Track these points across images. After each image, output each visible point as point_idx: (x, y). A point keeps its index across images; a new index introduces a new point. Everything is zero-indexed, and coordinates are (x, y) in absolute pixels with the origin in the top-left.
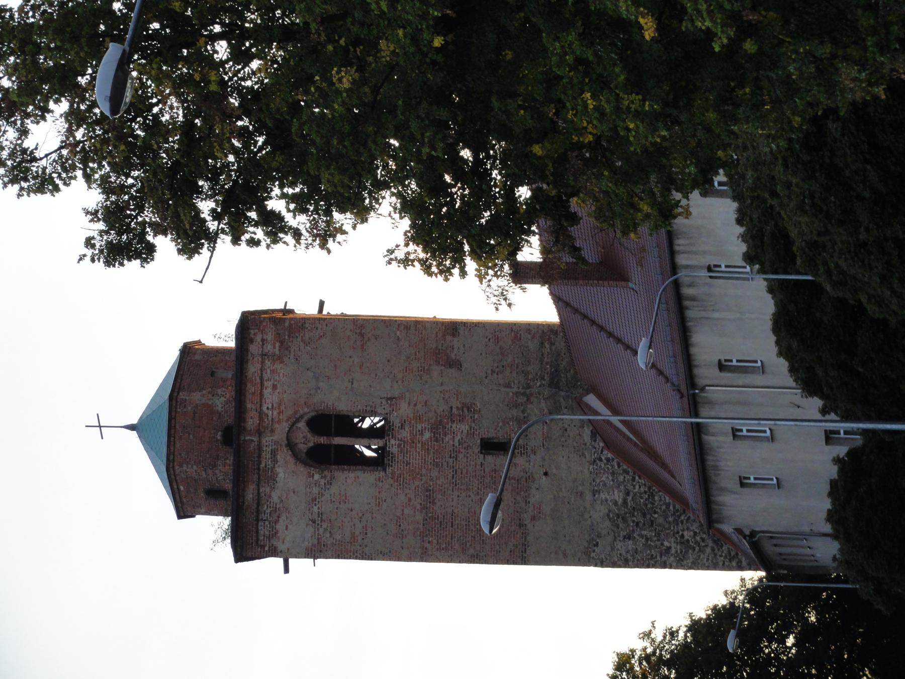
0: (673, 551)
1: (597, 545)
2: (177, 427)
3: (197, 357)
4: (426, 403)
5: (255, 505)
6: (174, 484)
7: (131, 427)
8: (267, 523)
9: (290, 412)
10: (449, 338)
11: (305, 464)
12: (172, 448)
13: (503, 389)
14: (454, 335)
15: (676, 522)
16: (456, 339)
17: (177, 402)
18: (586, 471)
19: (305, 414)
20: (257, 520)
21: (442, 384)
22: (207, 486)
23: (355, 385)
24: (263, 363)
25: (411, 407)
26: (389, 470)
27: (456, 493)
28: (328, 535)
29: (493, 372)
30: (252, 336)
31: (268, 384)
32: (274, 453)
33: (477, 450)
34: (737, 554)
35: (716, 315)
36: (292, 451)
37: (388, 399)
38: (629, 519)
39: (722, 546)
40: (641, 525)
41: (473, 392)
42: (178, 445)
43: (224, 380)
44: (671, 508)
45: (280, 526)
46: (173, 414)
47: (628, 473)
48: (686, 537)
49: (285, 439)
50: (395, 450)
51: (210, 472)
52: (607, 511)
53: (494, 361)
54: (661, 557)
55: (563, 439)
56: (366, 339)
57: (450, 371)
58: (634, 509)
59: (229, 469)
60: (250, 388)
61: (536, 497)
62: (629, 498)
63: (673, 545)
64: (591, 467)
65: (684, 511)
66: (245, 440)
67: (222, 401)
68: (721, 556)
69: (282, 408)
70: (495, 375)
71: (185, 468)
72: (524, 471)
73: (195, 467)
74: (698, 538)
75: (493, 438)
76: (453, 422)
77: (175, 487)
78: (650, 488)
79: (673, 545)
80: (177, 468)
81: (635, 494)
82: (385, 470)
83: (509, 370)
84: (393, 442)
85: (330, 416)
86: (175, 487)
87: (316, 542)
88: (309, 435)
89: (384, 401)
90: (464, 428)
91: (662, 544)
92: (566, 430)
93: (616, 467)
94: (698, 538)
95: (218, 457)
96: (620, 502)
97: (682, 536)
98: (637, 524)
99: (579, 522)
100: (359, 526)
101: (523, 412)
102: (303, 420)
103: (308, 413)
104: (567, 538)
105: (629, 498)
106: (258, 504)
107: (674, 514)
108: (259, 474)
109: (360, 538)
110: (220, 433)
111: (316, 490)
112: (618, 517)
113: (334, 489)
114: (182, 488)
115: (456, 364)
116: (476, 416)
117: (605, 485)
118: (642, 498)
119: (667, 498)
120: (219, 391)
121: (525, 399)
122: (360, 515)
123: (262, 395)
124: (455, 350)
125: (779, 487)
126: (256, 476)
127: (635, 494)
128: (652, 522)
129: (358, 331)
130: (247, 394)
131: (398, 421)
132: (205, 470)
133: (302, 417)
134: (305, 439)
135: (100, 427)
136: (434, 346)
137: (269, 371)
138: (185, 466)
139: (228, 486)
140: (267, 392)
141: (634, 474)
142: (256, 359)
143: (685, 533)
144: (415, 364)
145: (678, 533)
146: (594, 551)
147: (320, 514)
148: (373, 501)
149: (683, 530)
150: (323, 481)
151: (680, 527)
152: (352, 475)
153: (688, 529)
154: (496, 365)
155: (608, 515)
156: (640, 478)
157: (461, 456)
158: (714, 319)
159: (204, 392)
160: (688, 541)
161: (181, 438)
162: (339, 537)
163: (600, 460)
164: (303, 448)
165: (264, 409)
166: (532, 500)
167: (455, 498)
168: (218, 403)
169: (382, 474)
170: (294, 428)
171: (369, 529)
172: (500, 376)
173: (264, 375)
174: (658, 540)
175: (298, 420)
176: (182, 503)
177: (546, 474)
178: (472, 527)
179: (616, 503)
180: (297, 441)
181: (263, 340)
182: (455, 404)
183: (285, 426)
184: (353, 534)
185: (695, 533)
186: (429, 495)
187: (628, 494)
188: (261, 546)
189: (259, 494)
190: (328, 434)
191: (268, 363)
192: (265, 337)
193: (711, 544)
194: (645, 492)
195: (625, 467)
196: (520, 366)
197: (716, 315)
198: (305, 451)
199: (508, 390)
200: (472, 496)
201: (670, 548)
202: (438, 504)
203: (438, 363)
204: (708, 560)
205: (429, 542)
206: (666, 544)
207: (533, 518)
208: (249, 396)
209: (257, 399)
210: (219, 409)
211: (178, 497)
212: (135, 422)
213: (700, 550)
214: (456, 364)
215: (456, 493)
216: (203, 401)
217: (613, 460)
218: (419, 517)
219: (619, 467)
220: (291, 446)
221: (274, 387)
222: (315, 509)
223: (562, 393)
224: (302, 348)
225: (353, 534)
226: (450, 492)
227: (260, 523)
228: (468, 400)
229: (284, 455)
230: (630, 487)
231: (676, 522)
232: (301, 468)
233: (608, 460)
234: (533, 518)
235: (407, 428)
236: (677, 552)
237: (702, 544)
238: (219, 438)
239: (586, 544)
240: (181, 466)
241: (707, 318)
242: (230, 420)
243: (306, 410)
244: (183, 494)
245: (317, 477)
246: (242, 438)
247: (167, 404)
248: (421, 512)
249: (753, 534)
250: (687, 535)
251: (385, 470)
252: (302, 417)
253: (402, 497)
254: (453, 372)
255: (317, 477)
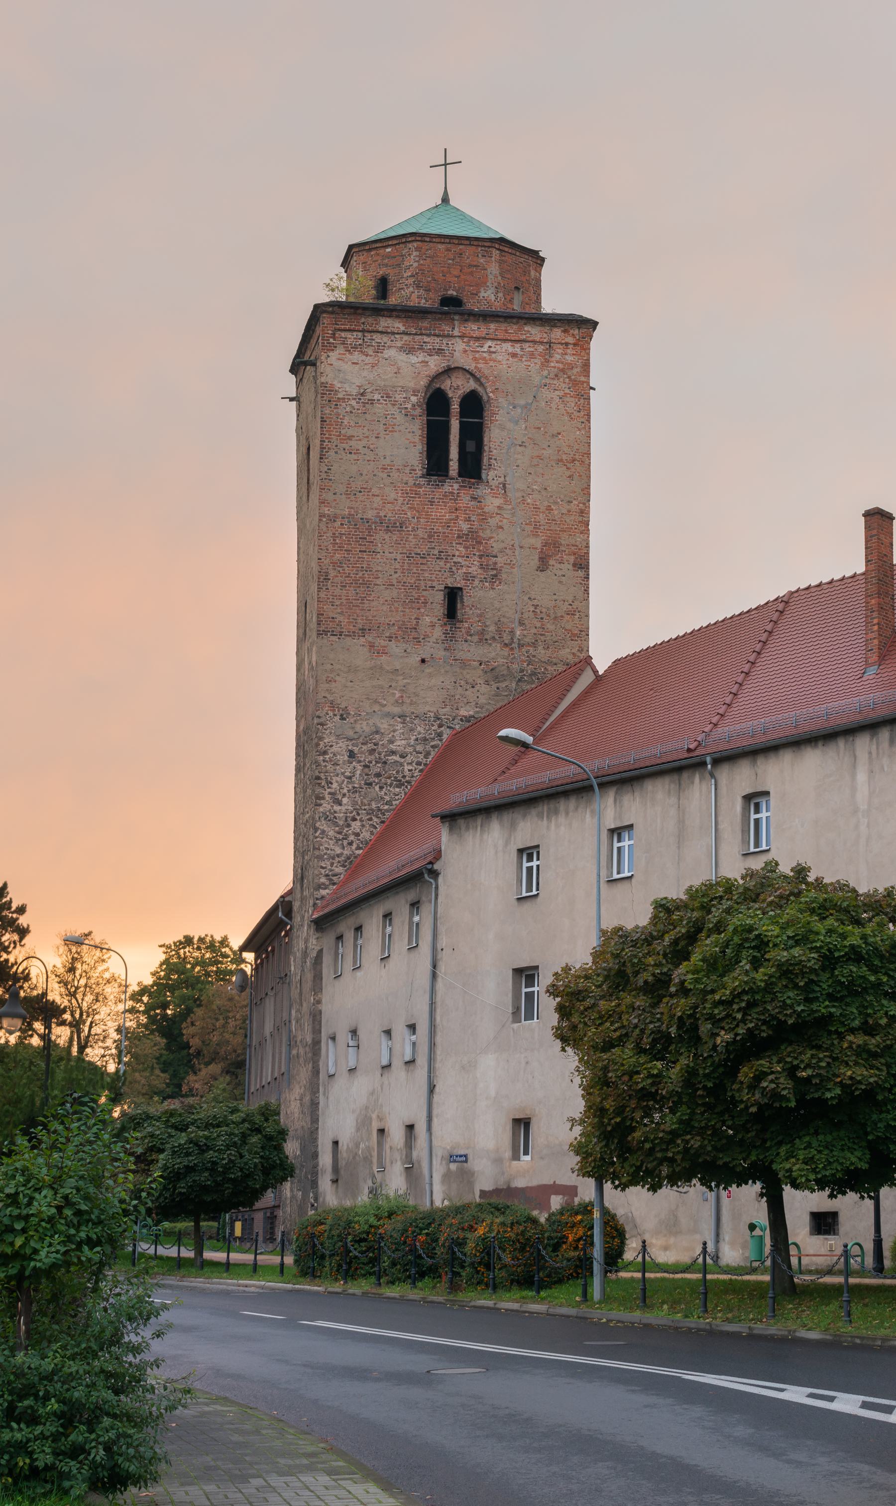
0: (337, 808)
1: (342, 718)
2: (461, 247)
3: (533, 273)
4: (501, 528)
5: (380, 329)
6: (395, 242)
7: (445, 200)
8: (360, 342)
9: (486, 372)
10: (572, 559)
11: (428, 387)
12: (437, 240)
13: (517, 616)
14: (574, 565)
15: (370, 812)
16: (571, 567)
17: (489, 247)
18: (427, 708)
19: (485, 389)
20: (363, 331)
21: (521, 547)
22: (391, 278)
23: (519, 449)
24: (542, 343)
25: (496, 510)
26: (422, 481)
27: (399, 557)
28: (348, 409)
29: (536, 606)
30: (571, 331)
31: (517, 349)
32: (440, 351)
33: (450, 582)
34: (334, 884)
35: (862, 777)
36: (442, 373)
37: (504, 485)
38: (373, 757)
39: (344, 866)
40: (367, 770)
41: (513, 583)
42: (440, 246)
43: (511, 301)
44: (386, 807)
45: (356, 356)
46: (476, 243)
47: (426, 756)
48: (353, 824)
49: (456, 365)
50: (447, 488)
51: (411, 281)
52: (383, 731)
53: (548, 609)
54: (330, 793)
55: (463, 683)
56: (569, 465)
57: (537, 557)
58: (385, 763)
59: (423, 303)
60: (512, 329)
61: (395, 648)
62: (397, 758)
63: (343, 808)
64: (432, 715)
65: (383, 822)
66: (453, 320)
67: (489, 297)
68: (332, 864)
69: (492, 364)
70: (532, 609)
71: (415, 253)
72: (426, 637)
73: (416, 264)
74: (352, 838)
75: (462, 602)
76: (481, 557)
77: (390, 243)
78: (409, 782)
79: (343, 808)
80: (415, 244)
81: (402, 765)
82: (423, 476)
83: (539, 625)
84: (456, 486)
85: (481, 416)
86: (390, 243)
87: (340, 396)
88: (460, 392)
89: (502, 479)
90: (475, 569)
91: (344, 795)
92: (473, 687)
93: (432, 744)
94: (352, 838)
95: (428, 290)
96: (392, 747)
97: (354, 819)
98: (366, 766)
99: (368, 699)
100: (359, 445)
101: (493, 638)
102: (477, 387)
103: (488, 393)
104: (350, 684)
105: (397, 758)
106: (382, 332)
107: (379, 810)
108: (416, 334)
109: (344, 445)
110: (455, 293)
111: (399, 397)
112: (375, 744)
113: (400, 418)
114: (389, 250)
115: (543, 564)
116: (487, 584)
117: (412, 730)
118: (398, 772)
119: (397, 802)
120: (500, 295)
121: (507, 642)
122: (371, 446)
123: (505, 340)
124: (559, 566)
125: (518, 899)
126: (414, 331)
127: (402, 765)
128: (370, 784)
129: (577, 457)
130: (506, 325)
131: (480, 494)
132: (412, 276)
133: (481, 384)
134: (456, 388)
135: (445, 165)
136: (563, 542)
137: (532, 349)
138: (418, 253)
139: (393, 300)
140: (507, 346)
141: (425, 765)
142: (545, 335)
143: (358, 823)
144: (542, 517)
145: (358, 814)
146: (335, 715)
147: (372, 401)
148: (389, 463)
149: (361, 820)
150: (409, 406)
151: (365, 818)
152: (417, 439)
153: (363, 826)
154: (544, 610)
155: (377, 732)
156: (421, 771)
157: (442, 563)
158: (853, 776)
159: (500, 278)
160: (349, 826)
161: (448, 250)
162: (346, 422)
163: (440, 726)
164: (446, 385)
165: (489, 343)
166: (393, 644)
167: (393, 556)
168: (489, 292)
169: (419, 473)
170: (468, 376)
171: (355, 457)
172: (531, 615)
173: (527, 344)
174: (349, 791)
175: (477, 380)
176: (370, 250)
177: (423, 661)
178: (360, 574)
179: (391, 742)
180: (453, 379)
181: (567, 344)
182: (500, 560)
183: (471, 366)
184: (350, 438)
185: (357, 835)
186: (396, 526)
187: (402, 756)
188: (334, 334)
189: (393, 333)
190: (463, 414)
191: (541, 348)
192: (571, 346)
193: (347, 852)
194: (404, 777)
195: (433, 754)
196: (543, 638)
197: (862, 777)
198: (443, 387)
199: (517, 621)
200: (397, 575)
201: (341, 805)
202: (386, 537)
203: (546, 544)
204: (327, 849)
205: (342, 524)
206: (345, 800)
207: (372, 646)
208: (503, 326)
209: (501, 335)
210: (482, 294)
211: (378, 245)
212: (452, 202)
213: (338, 840)
214: (543, 564)
215: (399, 557)
216: (490, 276)
217: (441, 740)
218: (370, 514)
219: (432, 747)
220: (449, 371)
221: (514, 355)
222: (377, 396)
223: (514, 685)
224: (557, 393)
225: (350, 438)
226: (400, 550)
227: (360, 334)
228: (504, 576)
229: (435, 364)
230: (409, 759)
231: (370, 812)
232: (423, 382)
233: (440, 735)
234: (372, 646)
235: (472, 503)
236: (335, 812)
237: (345, 842)
238: (449, 292)
239: (343, 706)
240: (417, 249)
241: (854, 766)
242: (471, 305)
243: (489, 390)
244: (381, 251)
245: (414, 399)
246: (457, 317)
247: (498, 236)
248: (377, 517)
249: (435, 874)
250: (356, 826)
251: (423, 476)
252: (481, 384)
253: (393, 495)
254: (535, 562)
255: (414, 399)
